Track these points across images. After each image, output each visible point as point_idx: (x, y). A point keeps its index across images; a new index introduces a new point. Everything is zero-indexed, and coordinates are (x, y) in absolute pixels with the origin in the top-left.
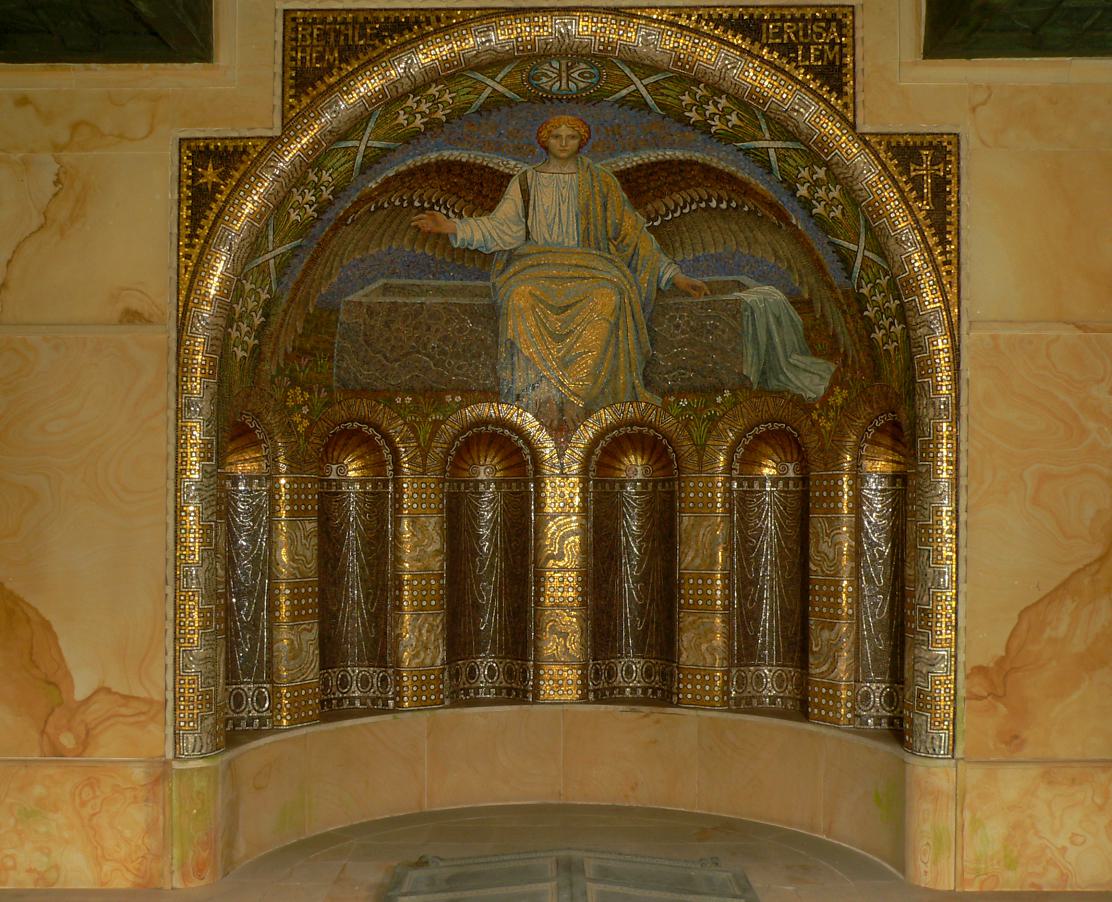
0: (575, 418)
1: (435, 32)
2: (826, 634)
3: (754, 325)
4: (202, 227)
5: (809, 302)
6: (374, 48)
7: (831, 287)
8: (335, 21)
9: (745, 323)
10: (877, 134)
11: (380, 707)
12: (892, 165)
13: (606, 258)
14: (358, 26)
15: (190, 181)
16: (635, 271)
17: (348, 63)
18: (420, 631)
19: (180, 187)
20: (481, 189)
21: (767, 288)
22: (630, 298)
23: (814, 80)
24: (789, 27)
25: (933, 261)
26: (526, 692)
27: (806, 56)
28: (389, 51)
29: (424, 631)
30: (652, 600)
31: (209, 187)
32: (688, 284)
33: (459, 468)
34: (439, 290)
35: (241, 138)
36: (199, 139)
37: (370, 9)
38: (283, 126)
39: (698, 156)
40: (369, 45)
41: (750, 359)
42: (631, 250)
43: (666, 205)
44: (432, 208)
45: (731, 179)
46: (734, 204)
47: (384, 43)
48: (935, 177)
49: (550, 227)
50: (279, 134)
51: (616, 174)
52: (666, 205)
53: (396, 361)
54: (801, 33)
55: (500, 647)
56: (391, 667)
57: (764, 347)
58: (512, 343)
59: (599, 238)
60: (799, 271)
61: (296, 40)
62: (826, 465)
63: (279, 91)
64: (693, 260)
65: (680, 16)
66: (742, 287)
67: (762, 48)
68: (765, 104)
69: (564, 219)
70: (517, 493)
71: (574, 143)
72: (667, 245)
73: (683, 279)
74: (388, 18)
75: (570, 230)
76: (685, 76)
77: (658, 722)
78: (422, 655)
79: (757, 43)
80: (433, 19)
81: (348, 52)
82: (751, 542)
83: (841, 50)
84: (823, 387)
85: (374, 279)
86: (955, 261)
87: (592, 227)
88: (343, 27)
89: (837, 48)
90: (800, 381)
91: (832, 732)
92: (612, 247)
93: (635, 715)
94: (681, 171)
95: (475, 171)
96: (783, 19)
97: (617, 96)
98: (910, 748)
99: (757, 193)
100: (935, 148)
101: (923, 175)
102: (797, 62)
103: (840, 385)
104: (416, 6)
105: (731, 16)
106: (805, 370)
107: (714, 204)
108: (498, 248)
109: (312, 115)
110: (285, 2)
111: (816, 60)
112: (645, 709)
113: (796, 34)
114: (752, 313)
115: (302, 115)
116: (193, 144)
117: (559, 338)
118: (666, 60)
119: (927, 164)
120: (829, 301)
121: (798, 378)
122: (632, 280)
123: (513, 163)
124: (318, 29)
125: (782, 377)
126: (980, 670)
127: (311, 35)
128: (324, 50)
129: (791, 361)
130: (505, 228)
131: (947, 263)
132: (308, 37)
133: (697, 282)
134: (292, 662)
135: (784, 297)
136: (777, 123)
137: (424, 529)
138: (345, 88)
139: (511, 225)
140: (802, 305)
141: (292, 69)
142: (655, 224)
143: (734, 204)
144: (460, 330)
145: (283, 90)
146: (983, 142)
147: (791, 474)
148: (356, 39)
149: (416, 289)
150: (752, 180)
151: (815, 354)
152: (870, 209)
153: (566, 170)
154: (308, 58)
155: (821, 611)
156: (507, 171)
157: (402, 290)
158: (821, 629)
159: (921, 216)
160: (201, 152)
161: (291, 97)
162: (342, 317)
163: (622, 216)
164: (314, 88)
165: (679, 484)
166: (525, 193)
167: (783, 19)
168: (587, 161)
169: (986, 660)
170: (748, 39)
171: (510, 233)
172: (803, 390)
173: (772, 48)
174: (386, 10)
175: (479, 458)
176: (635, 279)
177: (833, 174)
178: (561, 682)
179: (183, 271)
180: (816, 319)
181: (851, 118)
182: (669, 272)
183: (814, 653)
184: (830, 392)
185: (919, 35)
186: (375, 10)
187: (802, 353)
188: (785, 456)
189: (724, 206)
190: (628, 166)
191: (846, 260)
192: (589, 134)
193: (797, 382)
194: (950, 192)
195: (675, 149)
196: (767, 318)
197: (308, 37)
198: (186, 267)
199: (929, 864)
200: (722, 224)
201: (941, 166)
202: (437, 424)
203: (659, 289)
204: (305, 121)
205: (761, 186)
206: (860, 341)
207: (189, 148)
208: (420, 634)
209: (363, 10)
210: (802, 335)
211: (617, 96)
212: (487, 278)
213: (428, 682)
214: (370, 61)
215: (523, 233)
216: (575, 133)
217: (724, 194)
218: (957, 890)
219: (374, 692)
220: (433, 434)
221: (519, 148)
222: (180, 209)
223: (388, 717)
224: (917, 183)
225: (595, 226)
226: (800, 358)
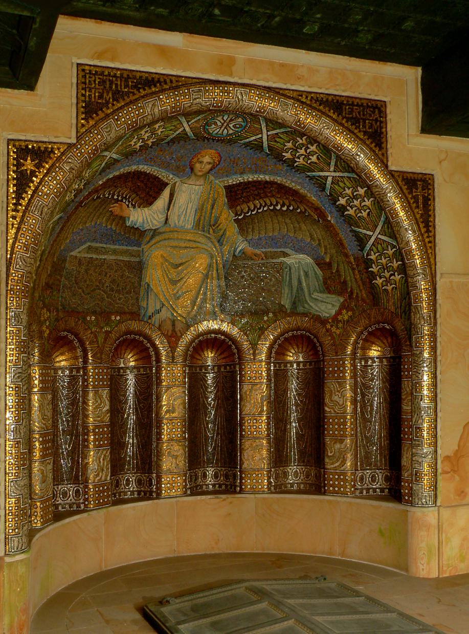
0: (181, 330)
1: (169, 89)
2: (337, 446)
3: (290, 276)
4: (24, 199)
5: (329, 265)
6: (134, 94)
7: (346, 256)
8: (109, 75)
9: (285, 275)
10: (397, 171)
11: (75, 509)
12: (404, 188)
13: (207, 237)
14: (123, 79)
15: (15, 168)
16: (221, 245)
17: (118, 101)
18: (99, 460)
19: (8, 171)
20: (147, 189)
21: (302, 256)
22: (216, 260)
23: (368, 139)
24: (356, 109)
25: (424, 241)
26: (151, 492)
27: (364, 127)
28: (143, 97)
29: (101, 460)
30: (218, 434)
31: (28, 172)
32: (252, 253)
33: (194, 358)
34: (115, 252)
35: (50, 143)
36: (21, 140)
37: (131, 70)
38: (77, 138)
39: (278, 179)
40: (131, 92)
41: (286, 295)
42: (222, 231)
43: (249, 207)
44: (122, 201)
45: (295, 193)
46: (291, 208)
47: (139, 92)
48: (424, 197)
49: (179, 216)
50: (75, 141)
51: (225, 187)
52: (249, 207)
53: (88, 294)
54: (361, 113)
55: (133, 467)
56: (82, 484)
57: (296, 289)
58: (148, 285)
59: (206, 224)
60: (325, 247)
61: (85, 83)
62: (336, 353)
63: (74, 115)
64: (258, 240)
65: (302, 96)
66: (285, 255)
67: (343, 119)
68: (341, 150)
69: (189, 211)
70: (143, 374)
71: (210, 166)
72: (244, 230)
73: (250, 250)
74: (142, 77)
75: (190, 220)
76: (297, 132)
77: (231, 503)
78: (101, 474)
79: (340, 116)
80: (168, 81)
81: (118, 95)
82: (367, 395)
83: (380, 124)
84: (334, 311)
85: (85, 242)
86: (433, 241)
87: (202, 218)
88: (114, 79)
89: (378, 123)
90: (318, 307)
91: (345, 499)
92: (211, 230)
93: (218, 500)
94: (265, 187)
95: (151, 180)
96: (353, 104)
97: (247, 140)
98: (411, 503)
99: (309, 201)
100: (424, 181)
101: (418, 195)
102: (359, 128)
103: (346, 309)
104: (158, 72)
105: (327, 99)
106: (322, 301)
107: (278, 207)
108: (148, 228)
109: (96, 132)
110: (79, 58)
111: (369, 128)
112: (224, 496)
113: (359, 113)
114: (290, 270)
115: (89, 131)
116: (17, 144)
117: (174, 282)
118: (292, 121)
119: (418, 188)
120: (343, 263)
121: (317, 306)
122: (219, 250)
123: (171, 176)
124: (99, 78)
125: (306, 305)
126: (447, 458)
127: (95, 81)
128: (103, 92)
129: (313, 296)
130: (155, 216)
131: (430, 242)
132: (92, 82)
133: (258, 251)
134: (43, 484)
135: (312, 261)
136: (344, 162)
137: (101, 397)
138: (116, 117)
139: (159, 214)
140: (320, 263)
141: (83, 101)
142: (240, 217)
143: (291, 208)
144: (122, 277)
145: (77, 114)
146: (445, 180)
147: (301, 359)
148: (123, 87)
149: (103, 250)
150: (309, 195)
151: (329, 292)
152: (392, 212)
153: (198, 183)
154: (93, 96)
155: (334, 433)
156: (166, 181)
157: (96, 250)
158: (334, 443)
159: (418, 216)
160: (23, 149)
161: (82, 119)
162: (67, 265)
163: (221, 212)
164: (97, 115)
165: (324, 364)
166: (172, 195)
167: (353, 104)
168: (212, 178)
169: (450, 452)
170: (336, 113)
171: (157, 219)
172: (320, 312)
173: (348, 120)
174: (140, 72)
175: (121, 355)
176: (221, 249)
177: (371, 192)
178: (174, 485)
179: (11, 227)
180: (333, 273)
181: (385, 162)
182: (242, 245)
183: (329, 457)
184: (339, 313)
185: (418, 121)
186: (134, 71)
187: (321, 292)
188: (298, 350)
189: (285, 209)
190: (234, 183)
191: (362, 241)
192: (219, 162)
193: (317, 308)
194: (430, 205)
195: (266, 174)
196: (299, 272)
197: (92, 82)
198: (13, 225)
199: (425, 565)
200: (280, 219)
201: (426, 191)
202: (107, 333)
203: (234, 255)
204: (92, 135)
205: (313, 198)
206: (363, 284)
207: (14, 146)
208: (100, 462)
209: (126, 70)
210: (322, 282)
211: (247, 140)
212: (139, 245)
213: (103, 491)
214: (131, 102)
215: (164, 219)
216: (212, 161)
217: (287, 202)
218: (441, 577)
219: (71, 500)
220: (105, 340)
221: (178, 167)
222: (8, 186)
223: (85, 515)
224: (415, 198)
225: (204, 217)
226: (319, 295)
